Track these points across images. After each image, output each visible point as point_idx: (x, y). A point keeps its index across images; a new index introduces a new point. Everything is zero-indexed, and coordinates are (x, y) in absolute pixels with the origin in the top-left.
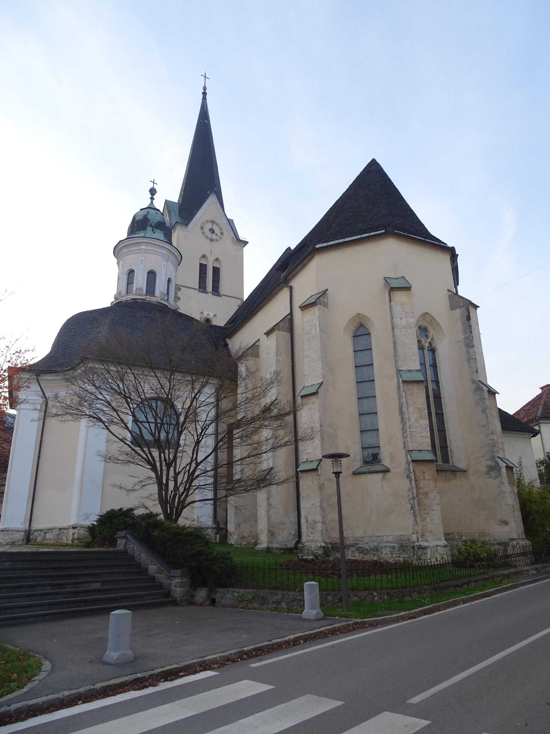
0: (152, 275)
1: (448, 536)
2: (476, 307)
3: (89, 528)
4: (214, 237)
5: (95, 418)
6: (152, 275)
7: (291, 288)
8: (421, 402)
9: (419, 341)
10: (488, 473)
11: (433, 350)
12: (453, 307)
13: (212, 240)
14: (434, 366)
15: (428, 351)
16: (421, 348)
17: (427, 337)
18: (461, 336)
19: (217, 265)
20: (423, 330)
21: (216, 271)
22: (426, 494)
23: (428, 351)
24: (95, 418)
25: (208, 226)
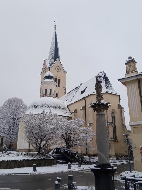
0: (51, 90)
1: (115, 154)
2: (123, 108)
3: (134, 170)
4: (59, 70)
5: (65, 141)
6: (51, 90)
7: (86, 100)
8: (112, 128)
9: (112, 115)
10: (124, 142)
11: (114, 117)
12: (119, 108)
13: (58, 72)
14: (114, 120)
15: (113, 117)
16: (112, 116)
17: (113, 114)
18: (120, 114)
19: (59, 79)
20: (113, 113)
21: (59, 80)
22: (112, 146)
23: (113, 117)
24: (65, 141)
25: (59, 70)
